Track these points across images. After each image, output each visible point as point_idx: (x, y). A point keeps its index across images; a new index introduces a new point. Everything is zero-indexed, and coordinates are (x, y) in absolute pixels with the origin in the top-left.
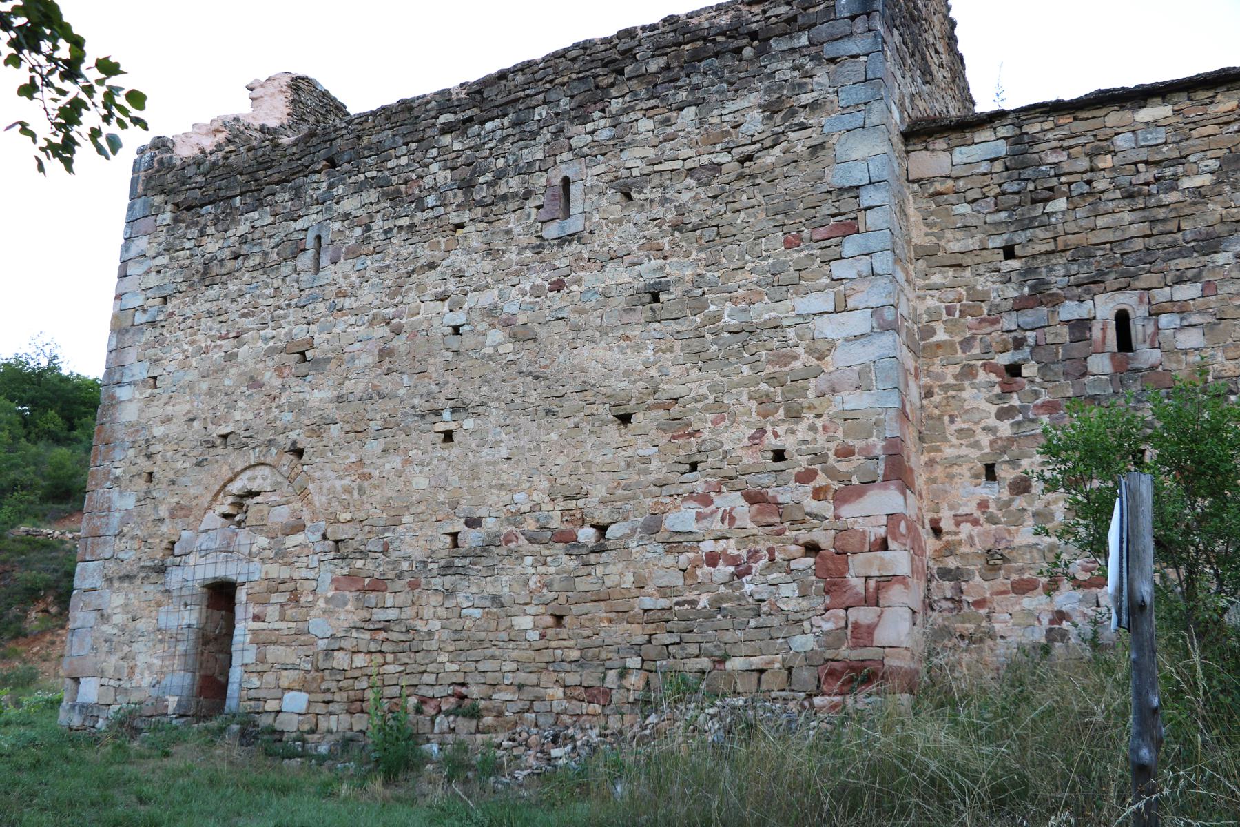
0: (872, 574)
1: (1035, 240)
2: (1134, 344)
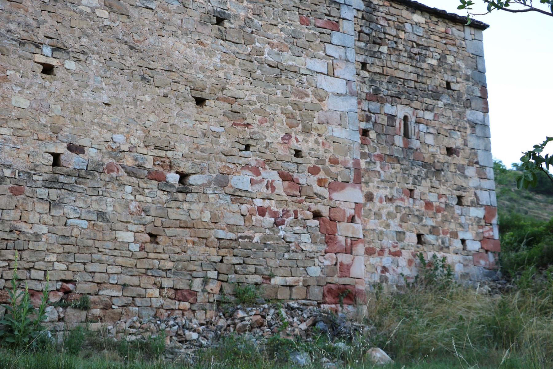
0: (349, 236)
2: (410, 135)
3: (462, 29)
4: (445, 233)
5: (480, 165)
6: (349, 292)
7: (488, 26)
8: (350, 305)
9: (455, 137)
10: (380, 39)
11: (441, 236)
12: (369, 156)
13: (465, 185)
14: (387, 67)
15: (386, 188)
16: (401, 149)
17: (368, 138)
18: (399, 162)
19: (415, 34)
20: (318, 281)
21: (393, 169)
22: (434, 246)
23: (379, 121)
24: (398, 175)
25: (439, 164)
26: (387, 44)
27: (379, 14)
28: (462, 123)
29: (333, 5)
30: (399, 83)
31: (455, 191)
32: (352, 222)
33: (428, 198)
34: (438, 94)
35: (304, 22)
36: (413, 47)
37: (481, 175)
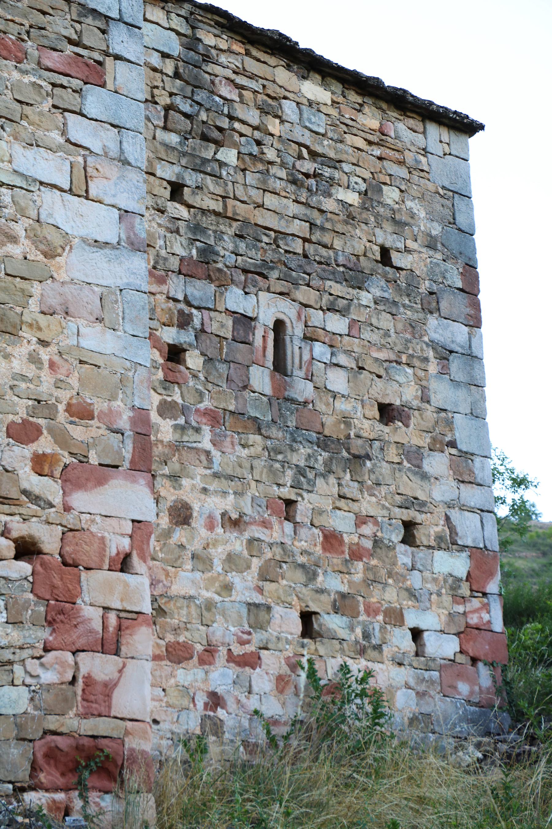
0: (113, 606)
1: (205, 190)
2: (289, 367)
3: (419, 127)
4: (371, 611)
5: (460, 451)
6: (107, 757)
7: (481, 127)
8: (106, 792)
9: (401, 379)
10: (220, 130)
11: (363, 617)
12: (184, 411)
13: (422, 496)
14: (235, 198)
15: (225, 493)
16: (265, 399)
17: (182, 368)
18: (259, 431)
19: (306, 127)
20: (19, 726)
21: (244, 446)
22: (345, 644)
23: (213, 328)
24: (256, 463)
25: (360, 442)
26: (235, 145)
27: (218, 70)
28: (417, 348)
29: (89, 20)
30: (265, 239)
31: (397, 510)
32: (122, 570)
33: (332, 523)
34: (360, 275)
35: (10, 52)
36: (300, 157)
37: (461, 475)
